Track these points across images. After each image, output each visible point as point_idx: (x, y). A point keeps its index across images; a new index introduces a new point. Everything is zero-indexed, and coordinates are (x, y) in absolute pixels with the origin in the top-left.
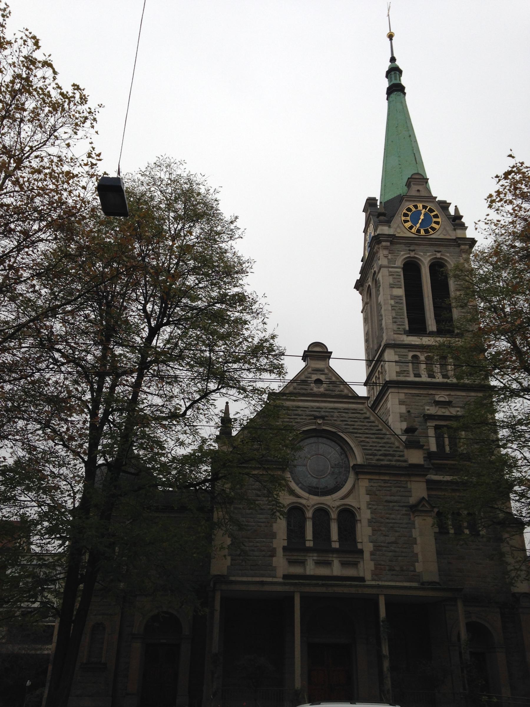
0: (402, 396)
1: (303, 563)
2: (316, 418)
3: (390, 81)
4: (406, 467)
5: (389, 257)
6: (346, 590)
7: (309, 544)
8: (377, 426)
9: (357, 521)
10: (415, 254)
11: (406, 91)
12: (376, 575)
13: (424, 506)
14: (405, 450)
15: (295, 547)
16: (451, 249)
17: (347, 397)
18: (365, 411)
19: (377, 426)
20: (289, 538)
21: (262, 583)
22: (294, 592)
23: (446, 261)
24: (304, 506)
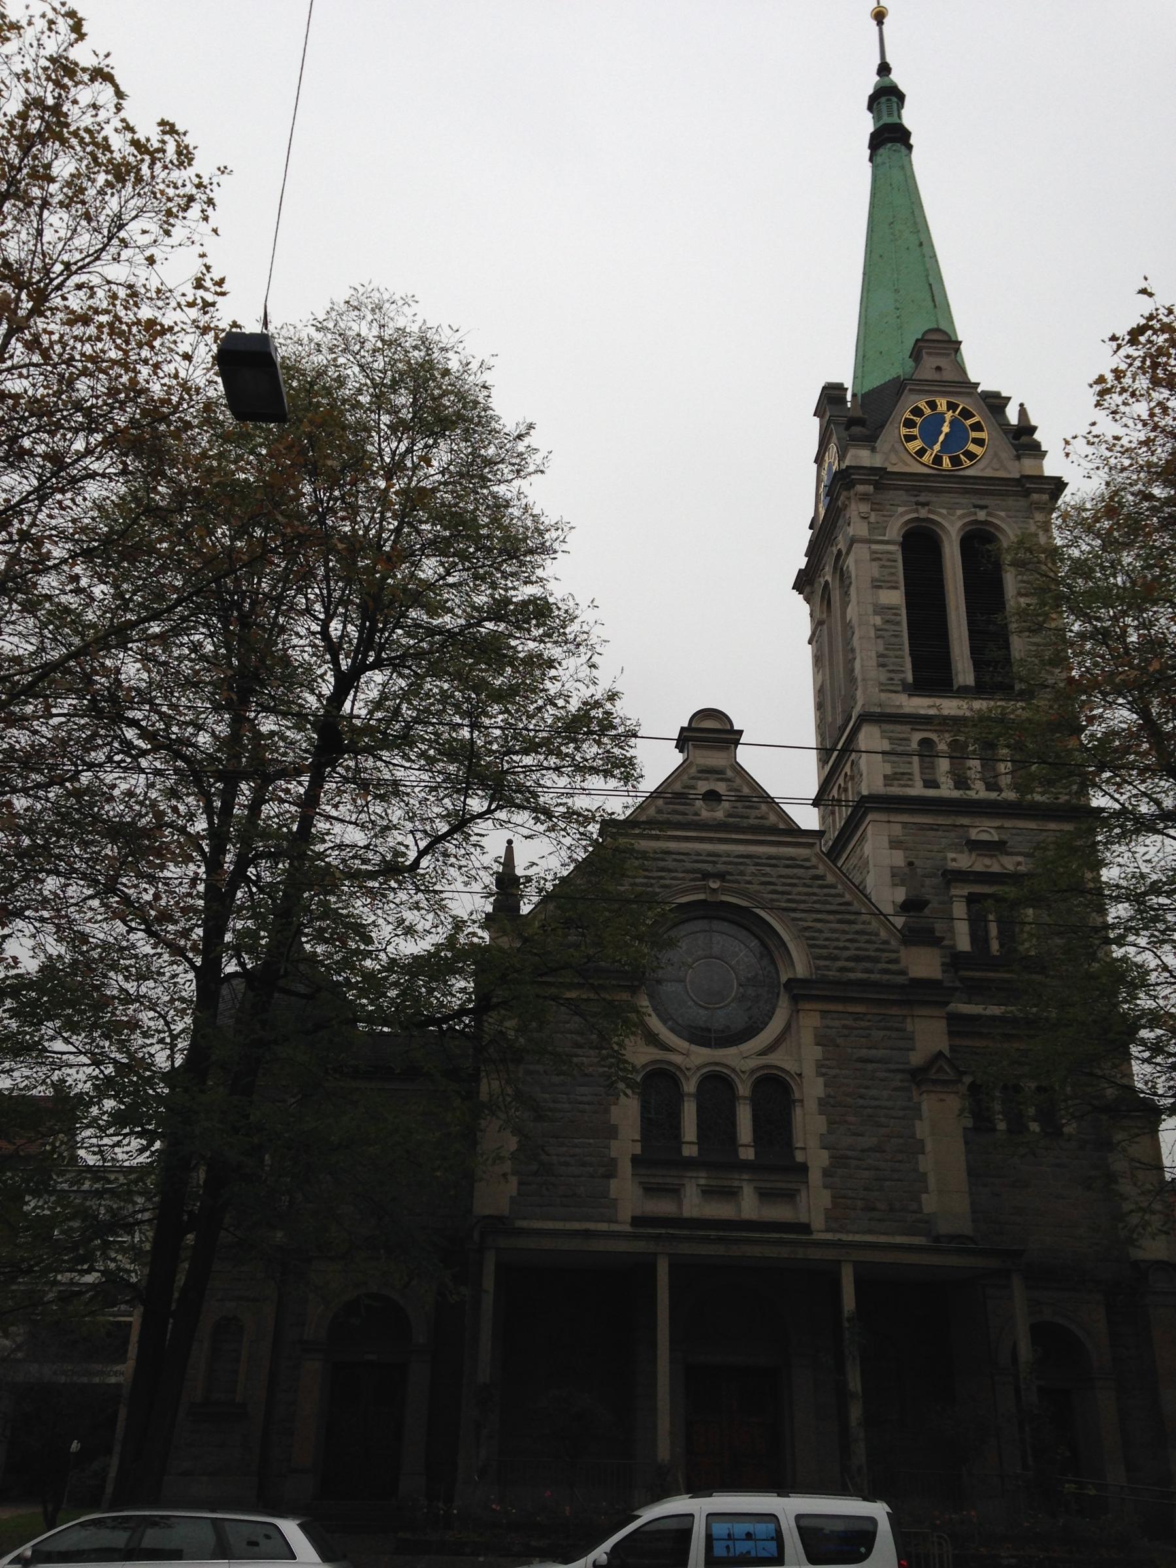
0: (897, 830)
2: (706, 876)
3: (876, 119)
5: (872, 519)
6: (756, 1251)
8: (842, 896)
9: (794, 1101)
10: (930, 512)
11: (912, 141)
14: (902, 948)
15: (659, 1157)
16: (1011, 502)
17: (773, 830)
18: (814, 861)
19: (842, 896)
21: (587, 1234)
24: (679, 1068)
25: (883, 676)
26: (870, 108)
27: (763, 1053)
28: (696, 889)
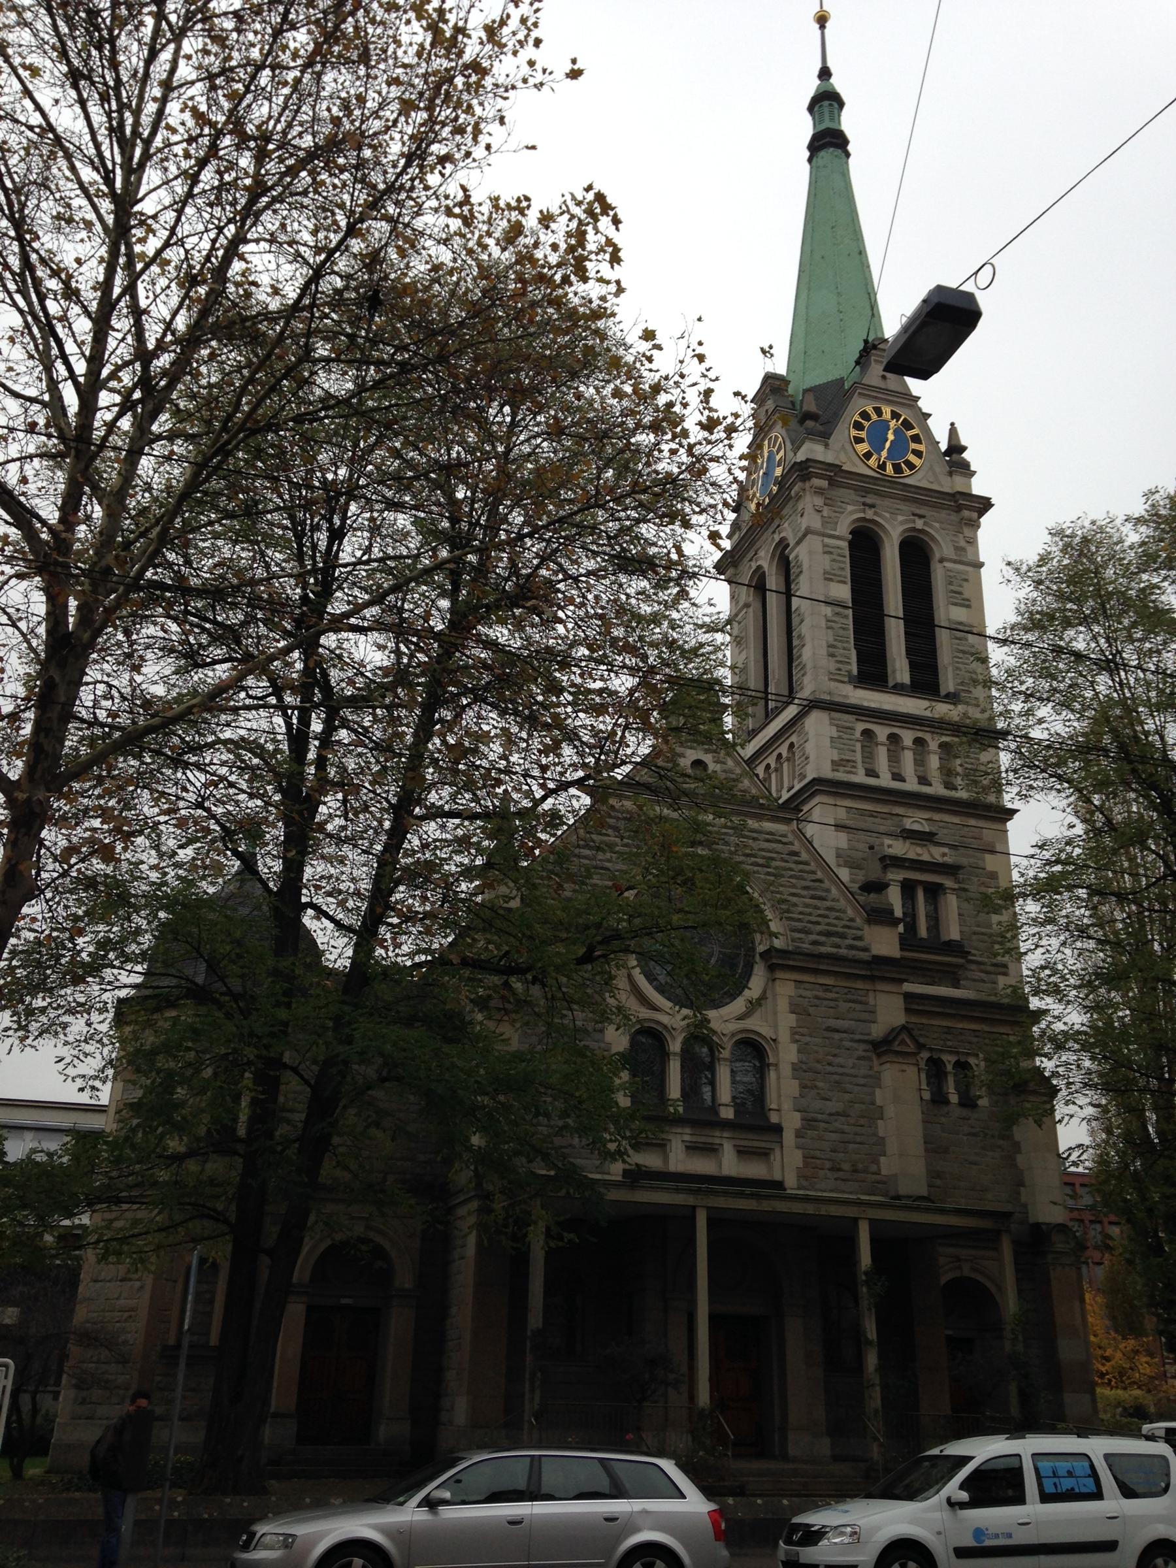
0: (842, 814)
1: (661, 1147)
5: (825, 514)
7: (727, 1113)
8: (814, 873)
9: (769, 1065)
10: (876, 513)
11: (850, 148)
13: (903, 1042)
14: (866, 927)
16: (943, 514)
18: (791, 838)
19: (814, 873)
23: (933, 538)
24: (665, 1027)
25: (833, 666)
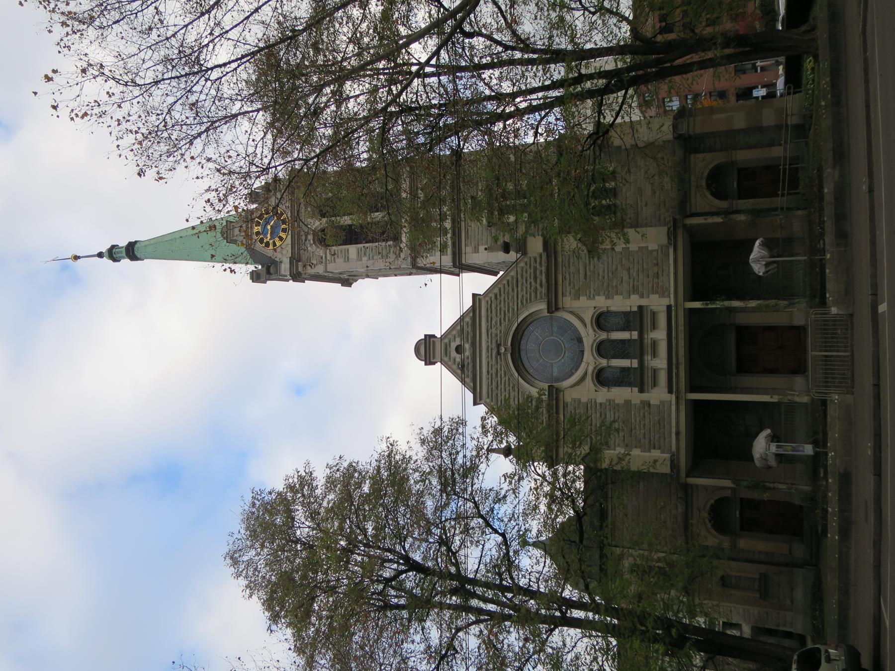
1: (655, 371)
2: (499, 353)
3: (124, 258)
4: (548, 256)
6: (682, 343)
12: (663, 293)
15: (638, 379)
17: (474, 318)
20: (630, 385)
21: (678, 433)
22: (684, 309)
24: (595, 368)
26: (119, 261)
27: (585, 325)
28: (506, 360)
